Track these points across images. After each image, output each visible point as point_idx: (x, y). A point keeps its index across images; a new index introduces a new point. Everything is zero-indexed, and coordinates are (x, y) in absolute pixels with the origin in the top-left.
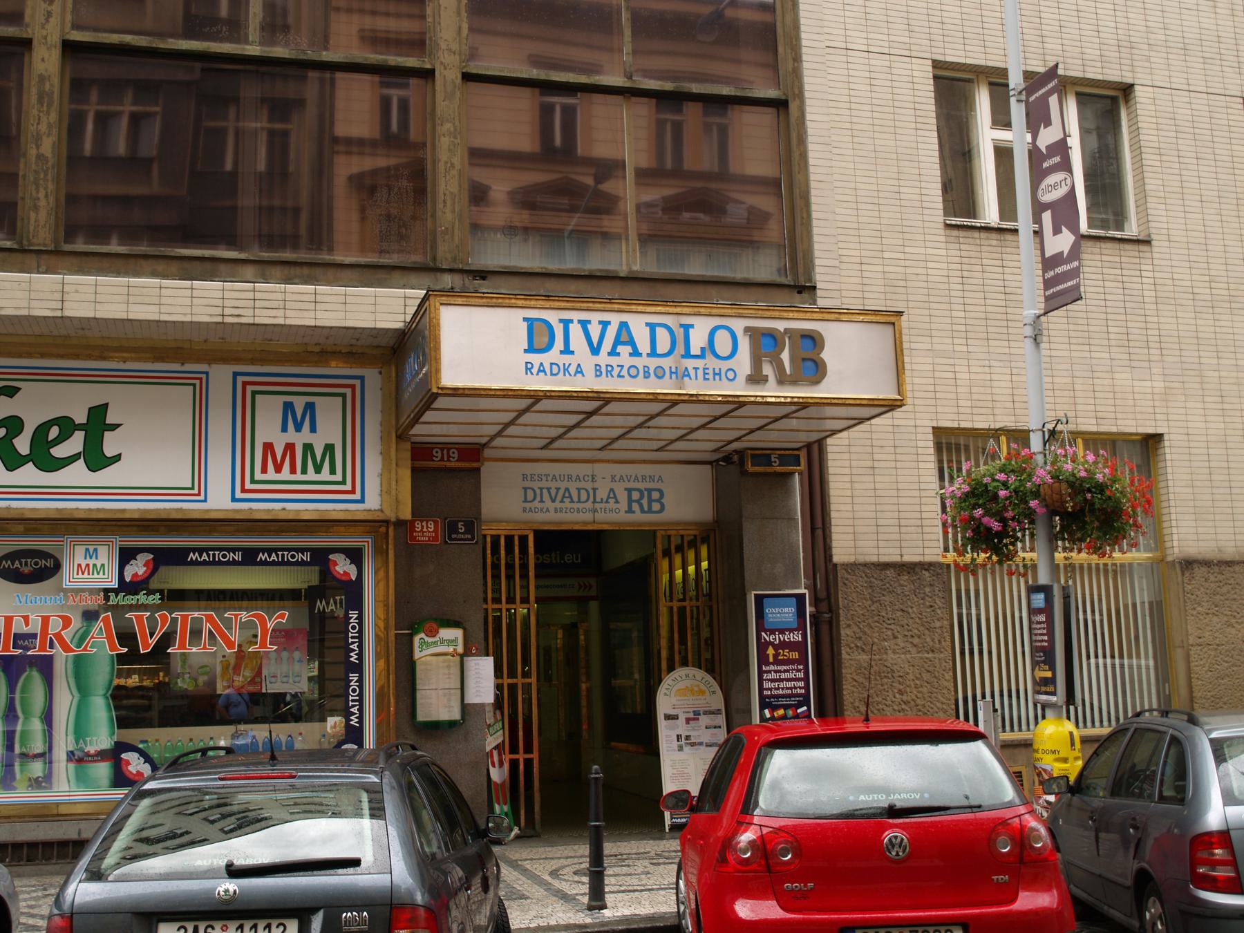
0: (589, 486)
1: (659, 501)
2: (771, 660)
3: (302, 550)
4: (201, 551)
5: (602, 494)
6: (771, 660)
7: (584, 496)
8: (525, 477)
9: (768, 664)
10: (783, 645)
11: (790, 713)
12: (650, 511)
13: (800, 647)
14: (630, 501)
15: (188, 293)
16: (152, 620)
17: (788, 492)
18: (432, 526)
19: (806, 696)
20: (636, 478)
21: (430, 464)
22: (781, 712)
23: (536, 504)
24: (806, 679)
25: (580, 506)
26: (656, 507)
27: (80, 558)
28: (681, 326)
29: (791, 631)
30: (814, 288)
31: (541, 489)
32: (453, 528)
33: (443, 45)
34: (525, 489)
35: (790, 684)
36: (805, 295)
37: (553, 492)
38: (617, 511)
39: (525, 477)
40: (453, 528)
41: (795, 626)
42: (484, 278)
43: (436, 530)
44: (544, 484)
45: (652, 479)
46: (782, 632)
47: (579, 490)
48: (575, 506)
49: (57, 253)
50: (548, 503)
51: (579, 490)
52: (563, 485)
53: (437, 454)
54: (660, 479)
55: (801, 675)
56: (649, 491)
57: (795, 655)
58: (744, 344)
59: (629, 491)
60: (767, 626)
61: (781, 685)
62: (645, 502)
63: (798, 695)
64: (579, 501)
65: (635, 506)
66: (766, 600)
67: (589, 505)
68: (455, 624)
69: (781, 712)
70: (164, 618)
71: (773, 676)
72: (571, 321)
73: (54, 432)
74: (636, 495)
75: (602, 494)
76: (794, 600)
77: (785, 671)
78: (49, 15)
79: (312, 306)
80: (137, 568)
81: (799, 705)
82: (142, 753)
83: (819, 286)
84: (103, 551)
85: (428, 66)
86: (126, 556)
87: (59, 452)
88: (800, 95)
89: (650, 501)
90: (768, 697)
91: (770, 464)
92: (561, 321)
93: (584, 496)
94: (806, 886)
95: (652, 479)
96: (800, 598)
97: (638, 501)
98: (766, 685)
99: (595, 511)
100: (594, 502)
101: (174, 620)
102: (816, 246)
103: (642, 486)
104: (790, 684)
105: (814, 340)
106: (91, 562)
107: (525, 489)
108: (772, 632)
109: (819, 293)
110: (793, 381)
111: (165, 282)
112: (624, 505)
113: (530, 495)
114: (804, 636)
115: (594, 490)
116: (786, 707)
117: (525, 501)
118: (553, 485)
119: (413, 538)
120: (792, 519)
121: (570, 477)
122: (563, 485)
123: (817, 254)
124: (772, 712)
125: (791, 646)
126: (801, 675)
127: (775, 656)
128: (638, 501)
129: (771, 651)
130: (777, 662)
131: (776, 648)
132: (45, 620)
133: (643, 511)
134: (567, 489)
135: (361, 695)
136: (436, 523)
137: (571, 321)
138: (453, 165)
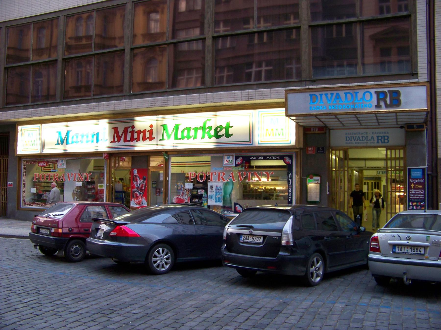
0: (365, 136)
1: (387, 139)
2: (413, 188)
3: (277, 156)
4: (253, 156)
5: (369, 138)
6: (413, 188)
7: (364, 138)
8: (346, 134)
9: (411, 189)
10: (417, 183)
11: (418, 204)
12: (384, 142)
13: (423, 184)
14: (378, 140)
15: (240, 94)
16: (242, 174)
17: (422, 136)
18: (313, 149)
19: (424, 199)
20: (380, 133)
21: (310, 132)
22: (415, 204)
23: (350, 141)
24: (424, 194)
25: (363, 141)
26: (386, 141)
27: (226, 159)
28: (355, 92)
29: (420, 179)
30: (417, 74)
31: (351, 137)
32: (318, 149)
33: (303, 19)
34: (346, 137)
35: (419, 195)
36: (415, 76)
37: (355, 138)
38: (374, 143)
39: (346, 134)
40: (318, 149)
41: (421, 177)
42: (315, 82)
43: (314, 150)
44: (352, 136)
45: (385, 133)
46: (417, 179)
47: (362, 137)
48: (361, 141)
49: (212, 88)
50: (353, 141)
51: (362, 137)
52: (357, 136)
53: (312, 129)
54: (388, 133)
55: (423, 193)
56: (384, 136)
57: (421, 187)
58: (375, 96)
59: (378, 137)
60: (412, 178)
61: (416, 195)
62: (383, 140)
63: (422, 199)
64: (362, 140)
65: (380, 141)
66: (412, 170)
67: (365, 141)
68: (317, 175)
69: (415, 204)
70: (245, 173)
71: (413, 192)
72: (322, 94)
73: (219, 129)
74: (380, 138)
75: (369, 138)
76: (421, 170)
77: (417, 191)
78: (209, 31)
79: (270, 94)
80: (239, 161)
81: (422, 202)
82: (240, 206)
83: (419, 73)
84: (231, 157)
85: (299, 25)
86: (236, 158)
87: (220, 134)
88: (415, 12)
89: (384, 140)
90: (411, 199)
91: (413, 128)
92: (320, 94)
93: (364, 138)
94: (48, 217)
95: (385, 133)
96: (423, 169)
97: (381, 140)
98: (410, 195)
99: (367, 143)
100: (367, 140)
101: (247, 174)
102: (419, 60)
103: (382, 135)
104: (419, 195)
105: (398, 93)
106: (229, 160)
107: (346, 137)
108: (413, 179)
109: (419, 75)
110: (391, 106)
111: (235, 92)
112: (376, 141)
113: (348, 139)
114: (425, 181)
115: (367, 137)
116: (417, 202)
117: (346, 140)
118: (355, 136)
119: (308, 152)
120: (423, 145)
121: (359, 133)
122: (357, 136)
123: (419, 63)
124: (412, 203)
125: (420, 184)
126: (423, 193)
127: (414, 187)
128: (381, 140)
129: (413, 185)
130: (415, 188)
131: (414, 184)
132: (219, 173)
133: (382, 142)
134: (359, 137)
135: (292, 194)
136: (314, 148)
137: (322, 94)
138: (306, 52)
